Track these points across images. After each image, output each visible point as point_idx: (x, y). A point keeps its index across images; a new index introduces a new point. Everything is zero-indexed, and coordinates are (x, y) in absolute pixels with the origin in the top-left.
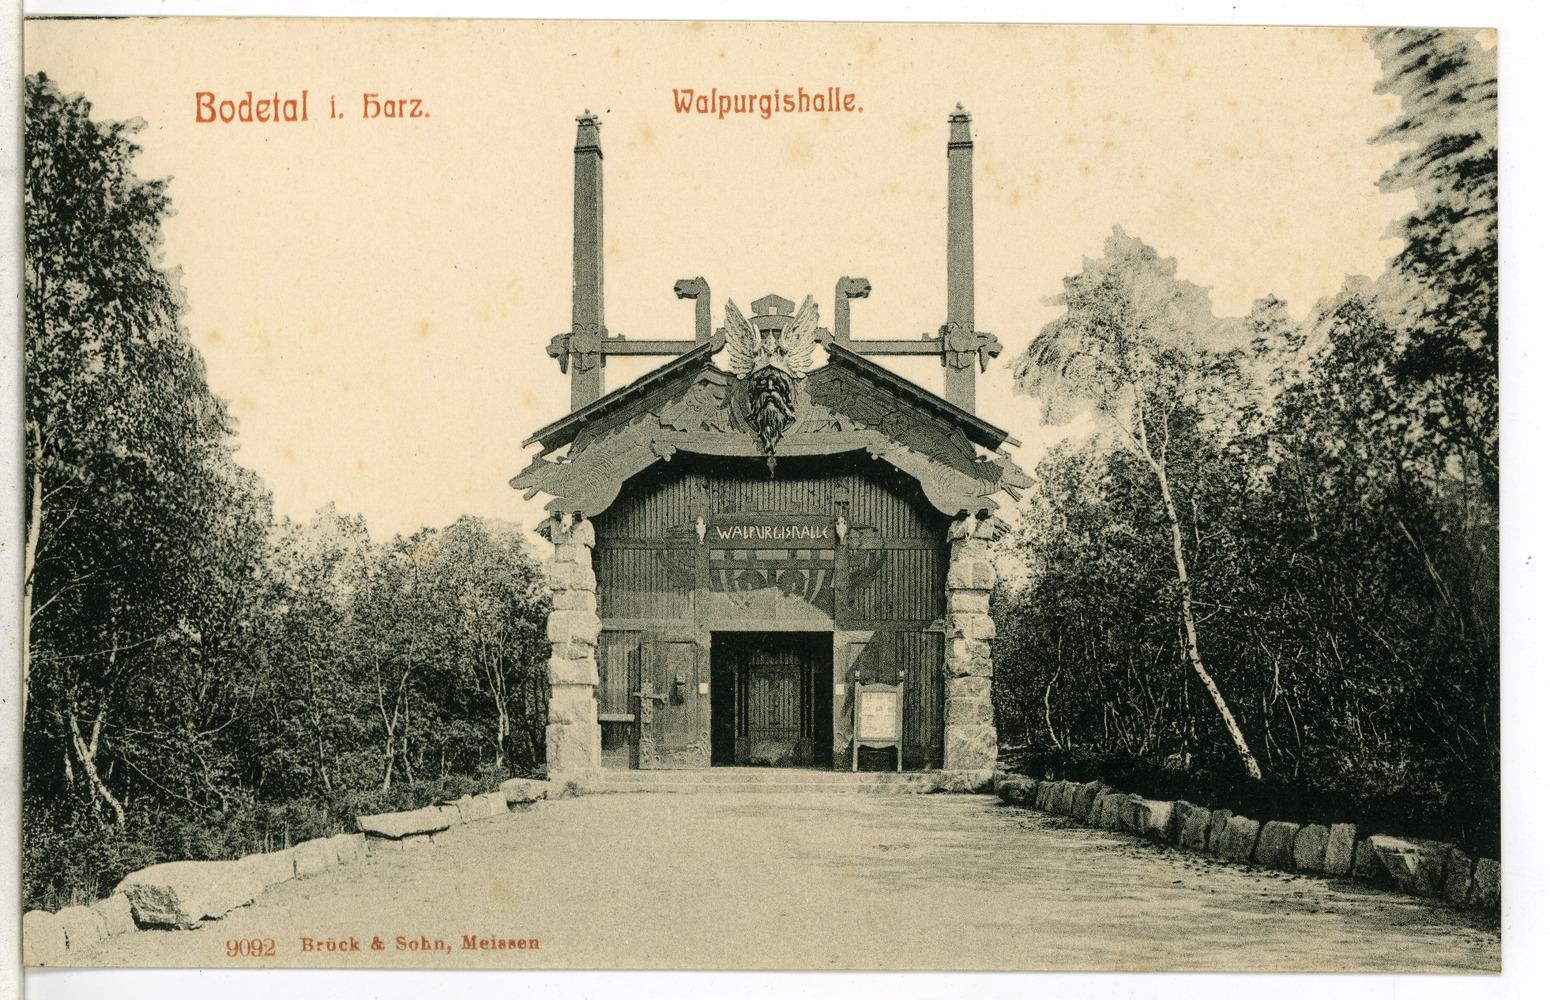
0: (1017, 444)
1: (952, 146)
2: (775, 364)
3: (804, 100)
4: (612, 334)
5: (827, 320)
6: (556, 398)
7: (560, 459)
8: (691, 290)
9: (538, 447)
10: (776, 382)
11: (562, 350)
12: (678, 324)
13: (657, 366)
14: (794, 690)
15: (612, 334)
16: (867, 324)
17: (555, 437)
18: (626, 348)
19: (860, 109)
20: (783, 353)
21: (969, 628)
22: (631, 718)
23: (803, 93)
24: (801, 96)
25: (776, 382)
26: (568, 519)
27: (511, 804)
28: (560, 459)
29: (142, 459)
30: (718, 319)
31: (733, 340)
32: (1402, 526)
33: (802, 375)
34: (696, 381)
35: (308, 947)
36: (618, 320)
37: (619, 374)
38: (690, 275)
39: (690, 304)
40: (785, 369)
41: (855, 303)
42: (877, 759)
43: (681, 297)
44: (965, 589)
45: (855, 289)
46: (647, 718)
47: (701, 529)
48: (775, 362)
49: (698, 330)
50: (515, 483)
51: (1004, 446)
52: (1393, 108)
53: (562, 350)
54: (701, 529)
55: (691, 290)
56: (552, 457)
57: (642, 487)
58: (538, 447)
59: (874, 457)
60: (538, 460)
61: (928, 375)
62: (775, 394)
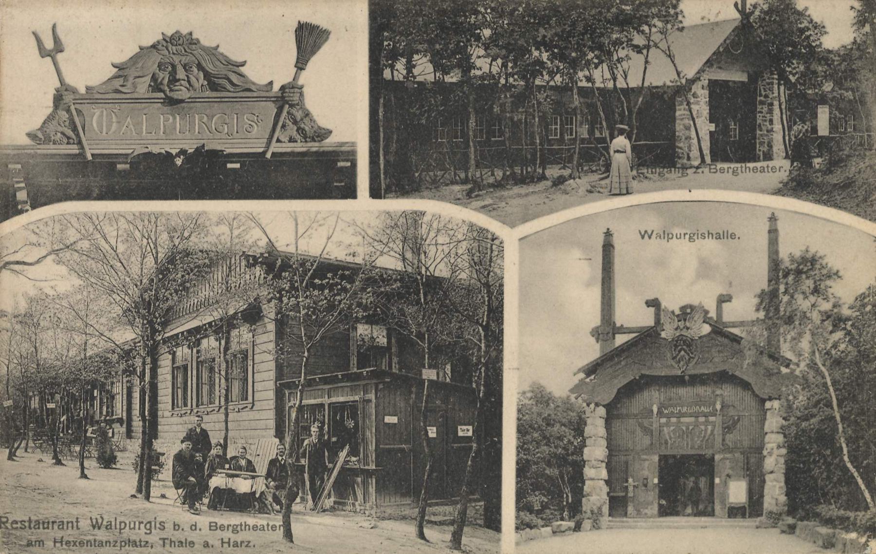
1: (770, 232)
2: (685, 334)
3: (247, 527)
4: (618, 325)
5: (713, 314)
6: (593, 351)
7: (591, 380)
9: (582, 375)
10: (684, 342)
11: (596, 333)
12: (646, 318)
13: (630, 338)
14: (706, 482)
15: (618, 325)
17: (592, 369)
18: (622, 330)
20: (688, 328)
22: (623, 494)
25: (684, 342)
26: (592, 406)
27: (554, 532)
28: (591, 380)
32: (456, 445)
33: (697, 338)
34: (781, 295)
37: (621, 339)
39: (652, 309)
40: (689, 336)
41: (725, 305)
42: (735, 512)
43: (648, 306)
44: (772, 432)
46: (631, 494)
47: (655, 409)
48: (684, 332)
52: (829, 265)
53: (596, 333)
54: (655, 409)
55: (654, 303)
57: (631, 390)
59: (730, 374)
62: (685, 347)
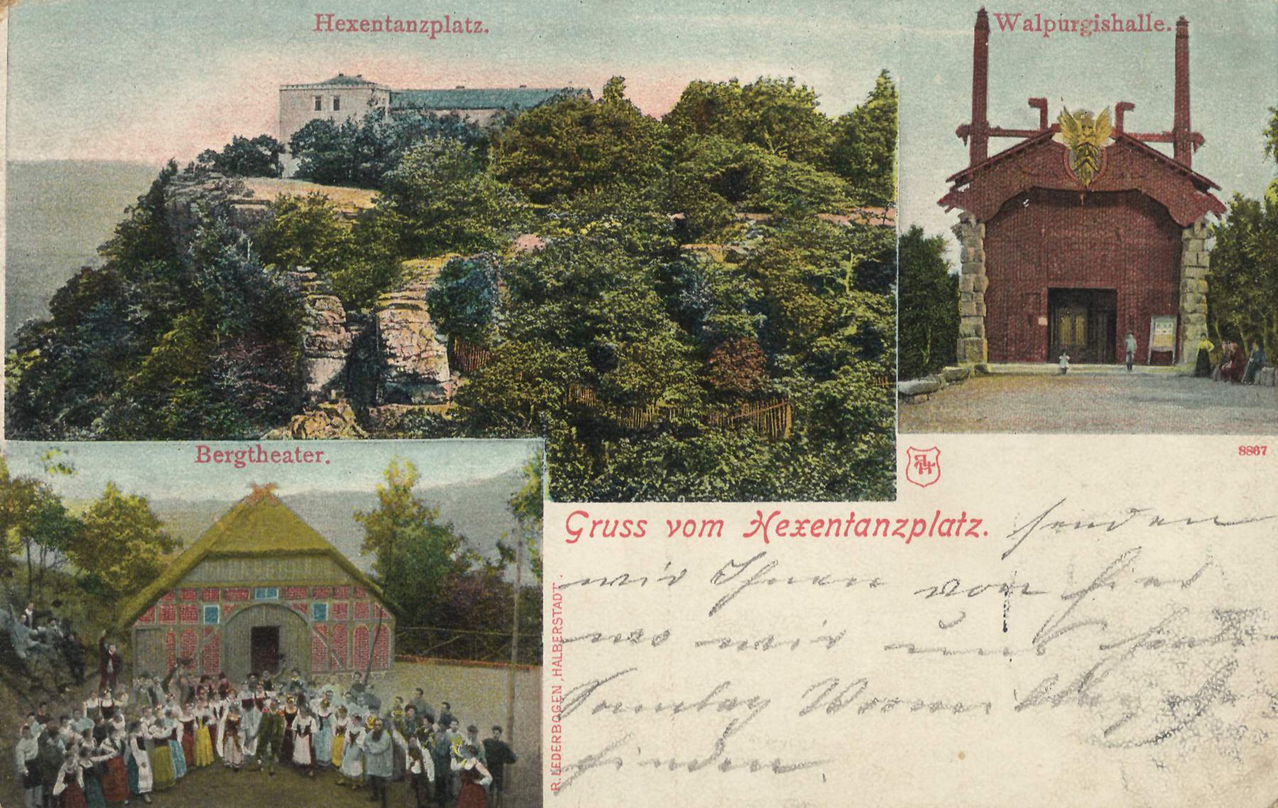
0: (1218, 188)
8: (1041, 104)
12: (1031, 120)
16: (1131, 125)
18: (999, 132)
19: (487, 31)
21: (438, 41)
23: (1117, 18)
24: (1115, 22)
29: (809, 271)
30: (1052, 120)
31: (1064, 127)
35: (412, 28)
36: (994, 118)
37: (996, 147)
38: (1039, 96)
41: (1126, 113)
45: (1122, 108)
49: (1165, 141)
50: (941, 203)
51: (1211, 190)
55: (1041, 104)
56: (962, 189)
58: (953, 183)
60: (952, 189)
61: (1167, 150)
